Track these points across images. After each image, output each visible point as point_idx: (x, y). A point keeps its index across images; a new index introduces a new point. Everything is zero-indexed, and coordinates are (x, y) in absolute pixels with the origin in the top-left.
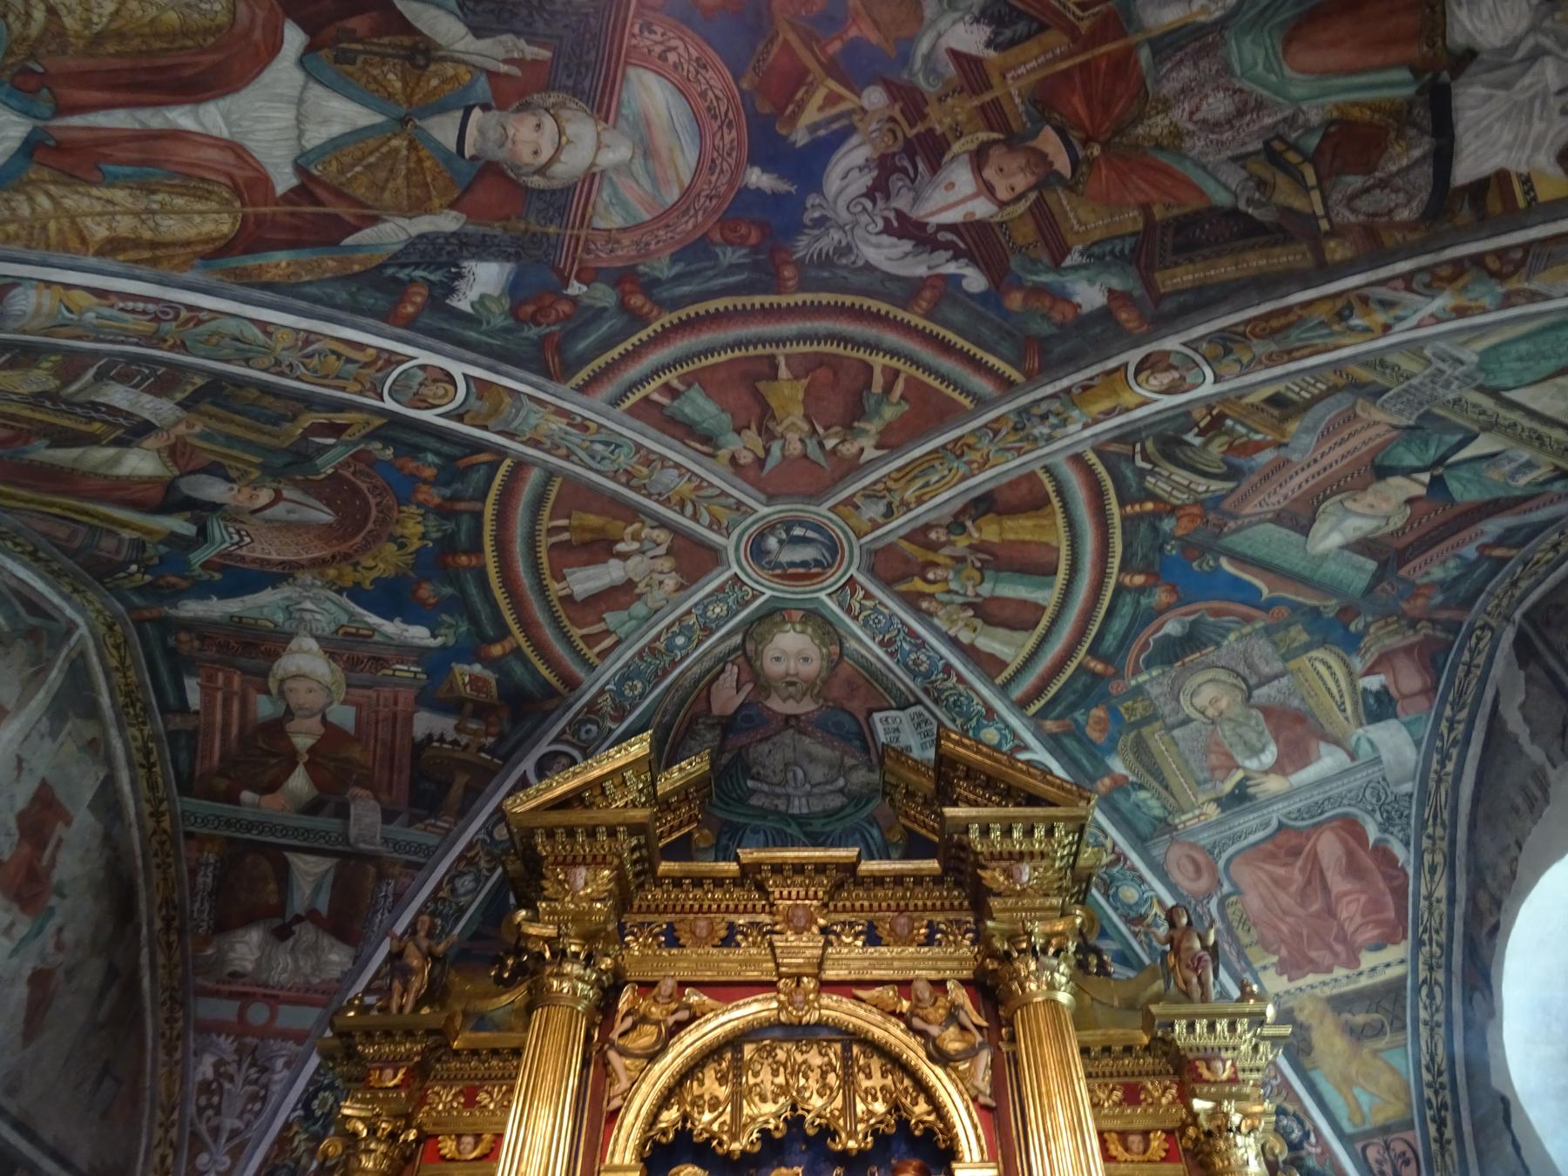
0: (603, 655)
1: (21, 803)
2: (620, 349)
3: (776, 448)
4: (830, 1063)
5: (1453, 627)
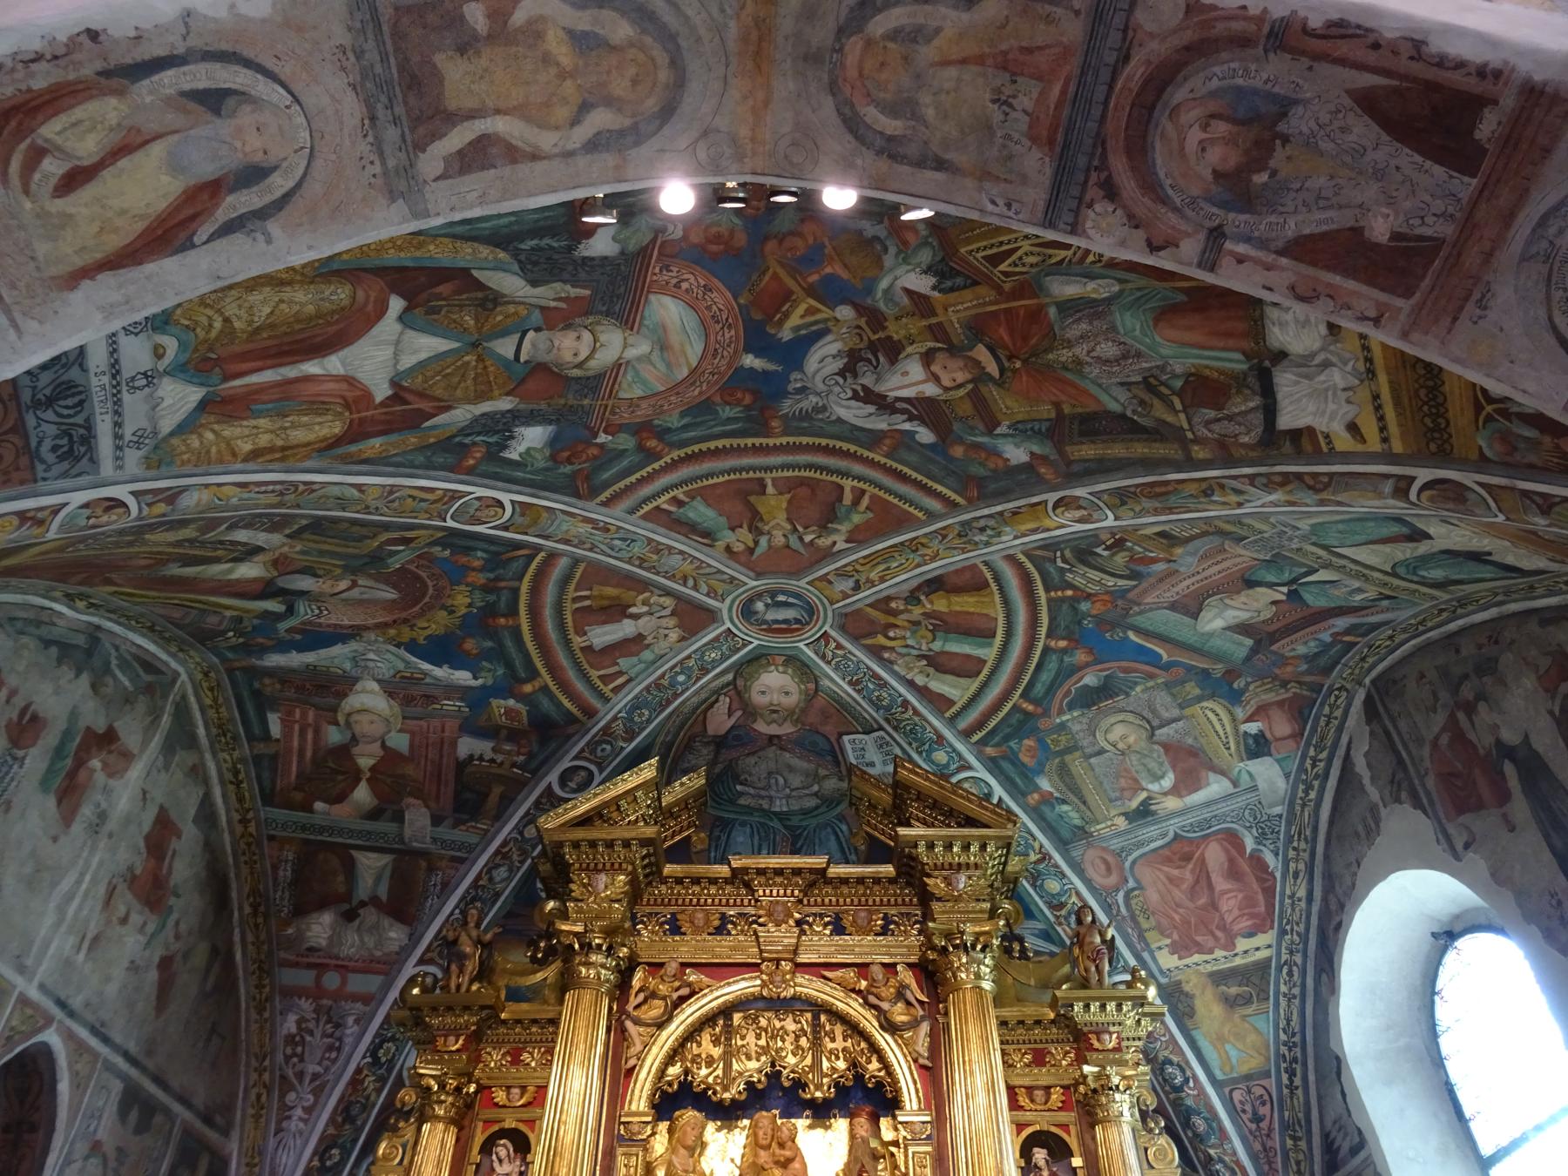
0: (616, 690)
1: (146, 828)
2: (638, 475)
3: (763, 541)
4: (802, 1029)
5: (1317, 688)
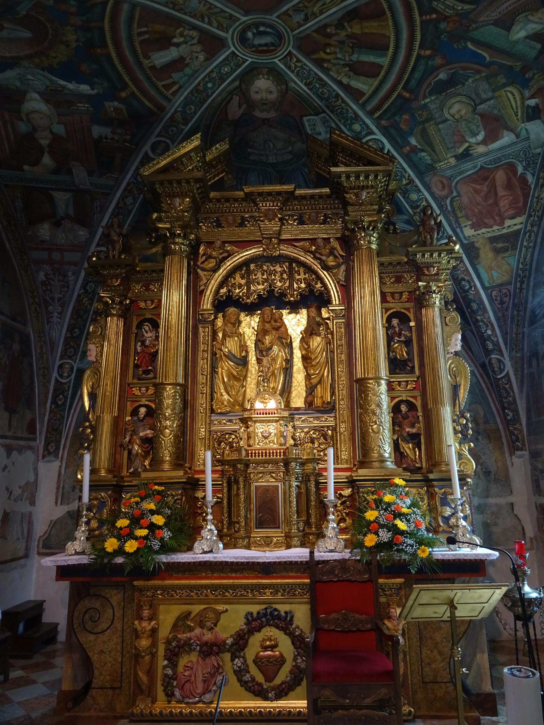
0: (174, 94)
4: (284, 270)
